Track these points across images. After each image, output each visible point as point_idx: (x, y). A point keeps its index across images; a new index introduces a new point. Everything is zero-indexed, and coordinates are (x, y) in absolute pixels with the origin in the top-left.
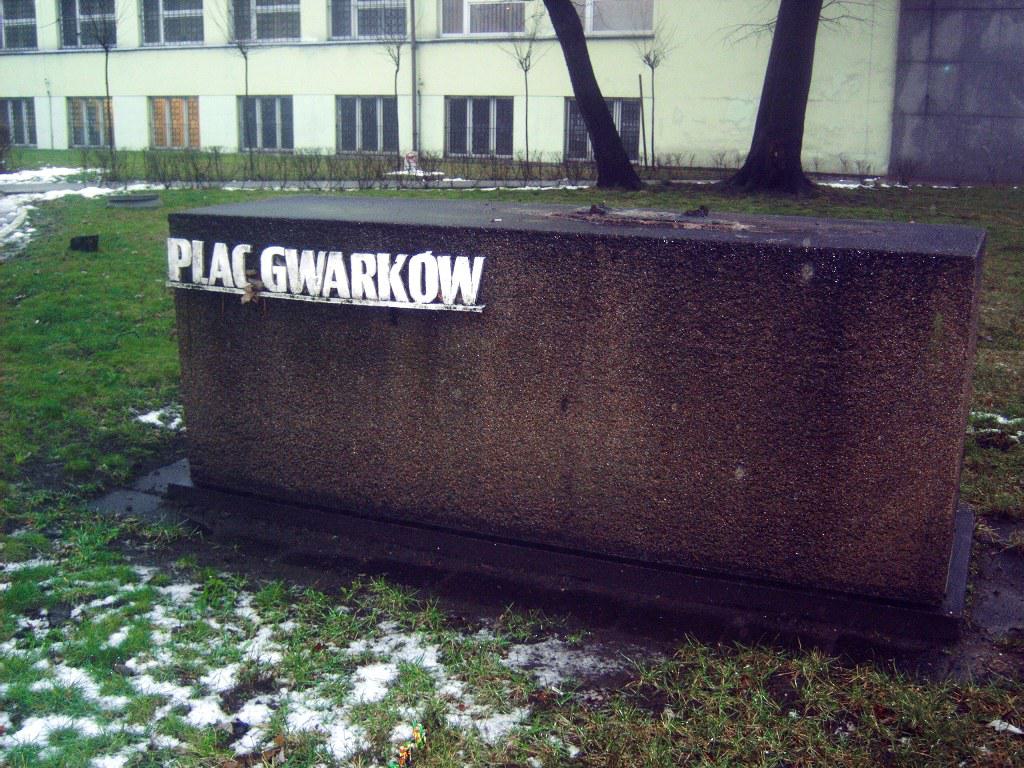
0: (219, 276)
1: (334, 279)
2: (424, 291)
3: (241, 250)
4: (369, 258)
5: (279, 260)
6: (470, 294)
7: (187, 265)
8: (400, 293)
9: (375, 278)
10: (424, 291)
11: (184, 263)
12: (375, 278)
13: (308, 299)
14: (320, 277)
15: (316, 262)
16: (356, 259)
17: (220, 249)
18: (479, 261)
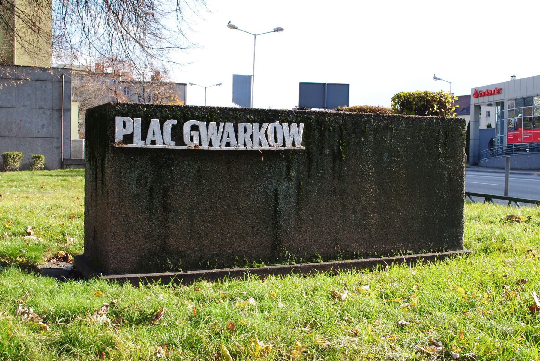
0: (228, 141)
1: (228, 137)
2: (276, 141)
3: (169, 124)
4: (249, 125)
5: (195, 128)
6: (299, 140)
7: (129, 132)
8: (264, 141)
9: (252, 136)
10: (276, 141)
11: (128, 132)
12: (252, 136)
13: (296, 148)
14: (220, 135)
15: (218, 129)
16: (241, 126)
17: (155, 123)
18: (302, 125)
